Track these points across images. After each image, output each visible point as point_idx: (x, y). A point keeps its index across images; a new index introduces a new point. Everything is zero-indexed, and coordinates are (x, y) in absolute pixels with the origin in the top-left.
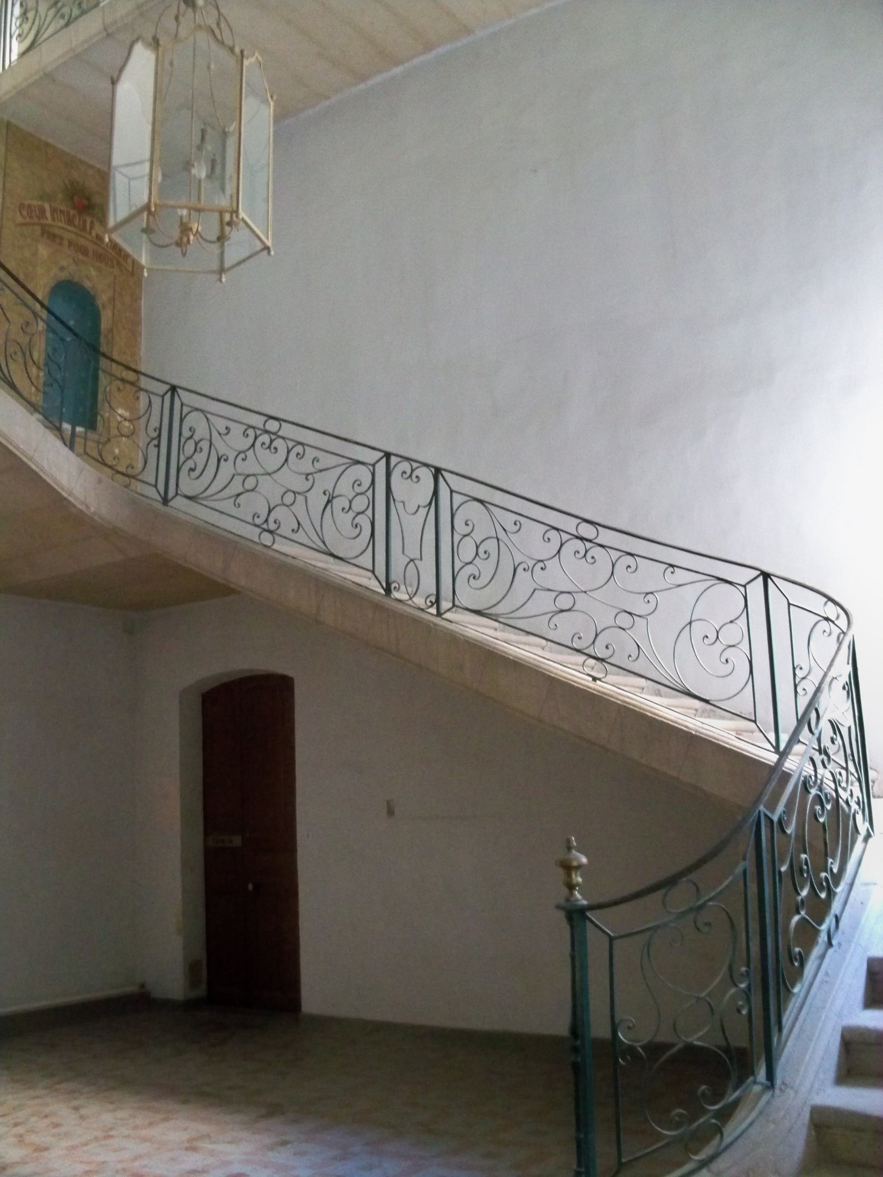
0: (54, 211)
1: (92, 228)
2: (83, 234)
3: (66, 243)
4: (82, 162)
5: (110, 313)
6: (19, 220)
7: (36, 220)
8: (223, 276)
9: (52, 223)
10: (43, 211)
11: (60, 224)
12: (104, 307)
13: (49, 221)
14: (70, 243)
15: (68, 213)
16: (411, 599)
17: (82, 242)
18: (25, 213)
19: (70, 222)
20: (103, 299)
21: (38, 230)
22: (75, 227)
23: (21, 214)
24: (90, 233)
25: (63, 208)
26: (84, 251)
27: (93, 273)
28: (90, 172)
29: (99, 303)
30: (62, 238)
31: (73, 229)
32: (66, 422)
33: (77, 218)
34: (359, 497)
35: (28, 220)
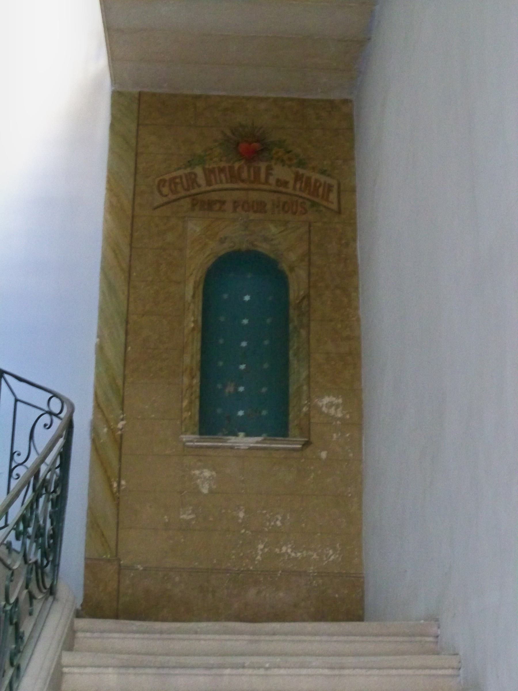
0: (209, 173)
1: (268, 174)
2: (255, 186)
3: (229, 206)
4: (248, 99)
5: (302, 273)
6: (159, 200)
7: (183, 193)
8: (167, 520)
9: (209, 188)
10: (192, 180)
11: (220, 186)
12: (292, 269)
13: (204, 188)
14: (236, 204)
15: (231, 168)
16: (57, 415)
17: (254, 196)
18: (165, 190)
19: (235, 177)
20: (290, 257)
21: (186, 203)
22: (243, 181)
23: (161, 194)
24: (267, 182)
25: (222, 164)
26: (260, 207)
27: (273, 229)
28: (263, 106)
29: (284, 266)
30: (223, 203)
31: (241, 185)
32: (327, 454)
33: (246, 168)
34: (21, 462)
35: (172, 197)
